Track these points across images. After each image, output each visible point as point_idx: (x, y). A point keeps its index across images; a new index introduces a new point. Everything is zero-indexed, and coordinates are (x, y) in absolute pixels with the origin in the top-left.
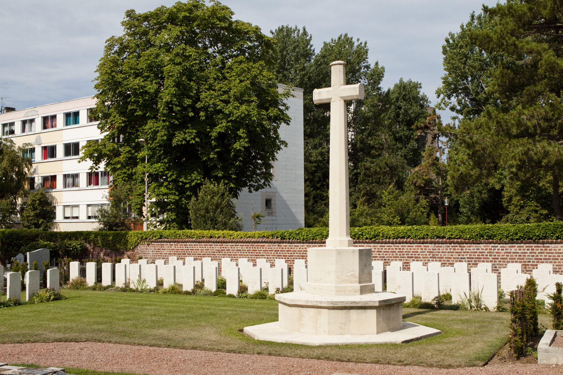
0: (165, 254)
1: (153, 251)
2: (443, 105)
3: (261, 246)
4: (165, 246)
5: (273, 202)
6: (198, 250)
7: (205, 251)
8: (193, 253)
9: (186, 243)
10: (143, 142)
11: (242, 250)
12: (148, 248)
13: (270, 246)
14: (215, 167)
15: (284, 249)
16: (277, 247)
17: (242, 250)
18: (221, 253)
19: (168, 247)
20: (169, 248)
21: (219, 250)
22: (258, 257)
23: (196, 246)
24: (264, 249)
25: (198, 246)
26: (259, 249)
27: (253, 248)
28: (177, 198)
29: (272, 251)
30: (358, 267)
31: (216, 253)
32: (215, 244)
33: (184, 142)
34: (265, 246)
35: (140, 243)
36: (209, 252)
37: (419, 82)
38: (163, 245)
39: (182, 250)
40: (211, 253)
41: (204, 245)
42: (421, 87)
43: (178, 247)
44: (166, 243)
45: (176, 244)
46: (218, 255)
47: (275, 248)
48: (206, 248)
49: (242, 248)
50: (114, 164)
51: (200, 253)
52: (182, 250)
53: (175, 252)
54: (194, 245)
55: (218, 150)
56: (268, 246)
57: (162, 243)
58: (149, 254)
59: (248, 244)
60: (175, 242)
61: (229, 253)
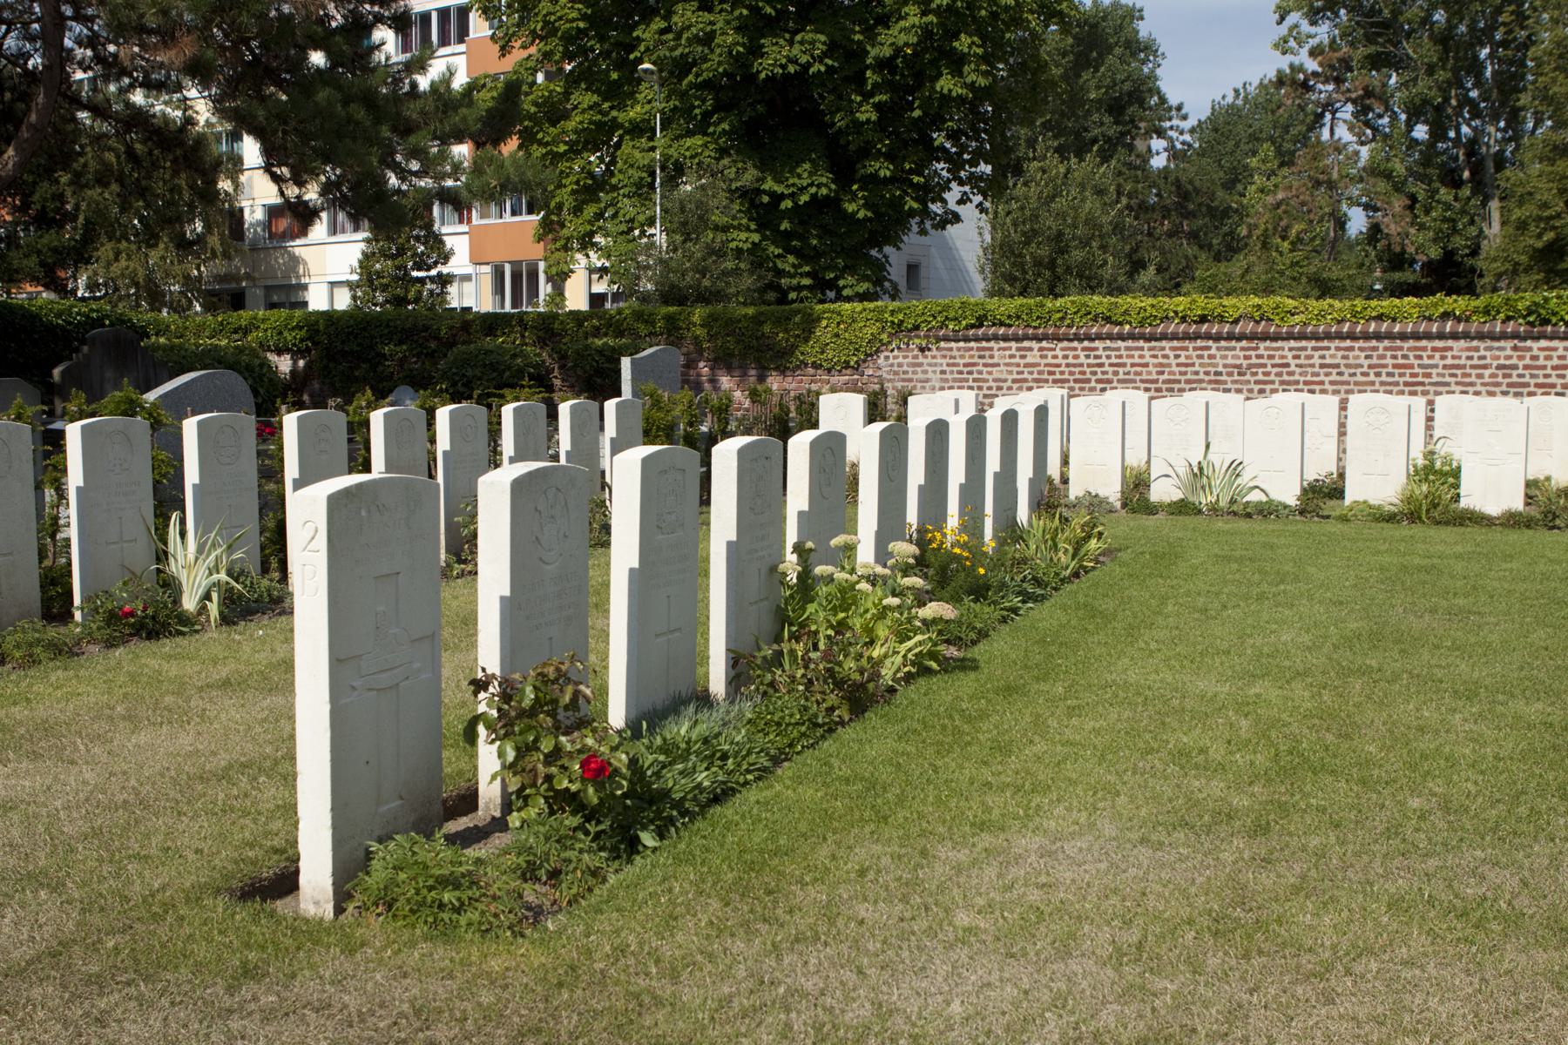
0: (995, 380)
1: (943, 372)
2: (1292, 43)
3: (1434, 349)
4: (996, 353)
5: (923, 272)
6: (1146, 365)
7: (1177, 369)
8: (1121, 376)
9: (1092, 340)
10: (652, 72)
11: (1347, 366)
12: (921, 360)
13: (1477, 349)
14: (866, 152)
15: (1541, 362)
16: (1509, 352)
17: (1347, 366)
18: (1248, 377)
19: (1012, 356)
20: (1017, 360)
21: (1239, 366)
22: (1419, 388)
23: (1136, 353)
24: (1449, 361)
25: (1145, 352)
26: (1426, 361)
27: (1394, 357)
28: (756, 237)
29: (1485, 367)
30: (736, 464)
31: (1224, 378)
32: (1223, 343)
33: (791, 69)
34: (1451, 349)
35: (890, 343)
36: (1197, 373)
37: (1138, 6)
38: (991, 349)
39: (1074, 365)
40: (1202, 376)
41: (1173, 349)
42: (1142, 18)
43: (1055, 357)
44: (1002, 344)
45: (1044, 344)
46: (1234, 382)
47: (1498, 358)
48: (1182, 360)
49: (1344, 357)
50: (547, 144)
51: (1155, 377)
52: (1074, 365)
53: (1040, 373)
54: (1127, 349)
55: (884, 98)
56: (1469, 349)
57: (984, 344)
58: (927, 381)
59: (1374, 343)
60: (1039, 340)
61: (1285, 377)
